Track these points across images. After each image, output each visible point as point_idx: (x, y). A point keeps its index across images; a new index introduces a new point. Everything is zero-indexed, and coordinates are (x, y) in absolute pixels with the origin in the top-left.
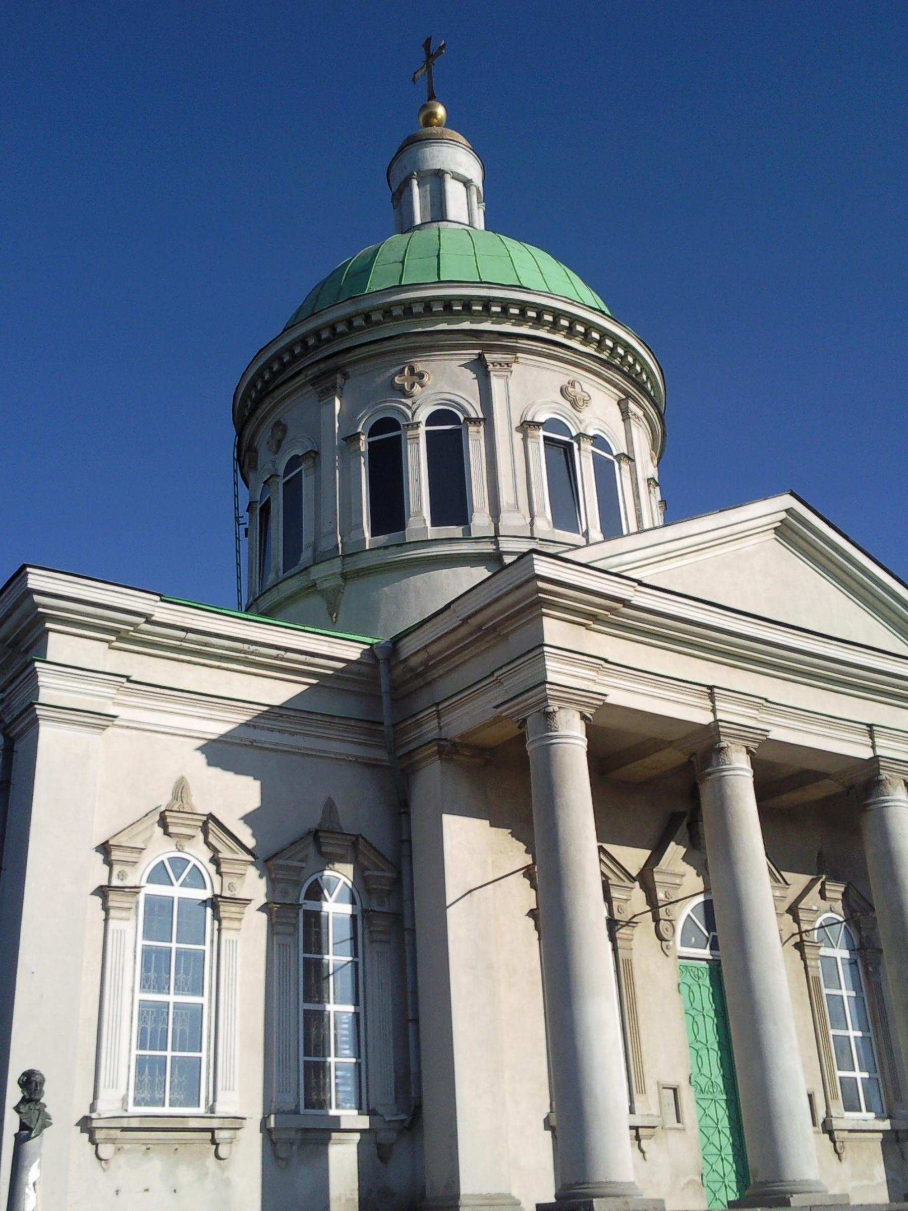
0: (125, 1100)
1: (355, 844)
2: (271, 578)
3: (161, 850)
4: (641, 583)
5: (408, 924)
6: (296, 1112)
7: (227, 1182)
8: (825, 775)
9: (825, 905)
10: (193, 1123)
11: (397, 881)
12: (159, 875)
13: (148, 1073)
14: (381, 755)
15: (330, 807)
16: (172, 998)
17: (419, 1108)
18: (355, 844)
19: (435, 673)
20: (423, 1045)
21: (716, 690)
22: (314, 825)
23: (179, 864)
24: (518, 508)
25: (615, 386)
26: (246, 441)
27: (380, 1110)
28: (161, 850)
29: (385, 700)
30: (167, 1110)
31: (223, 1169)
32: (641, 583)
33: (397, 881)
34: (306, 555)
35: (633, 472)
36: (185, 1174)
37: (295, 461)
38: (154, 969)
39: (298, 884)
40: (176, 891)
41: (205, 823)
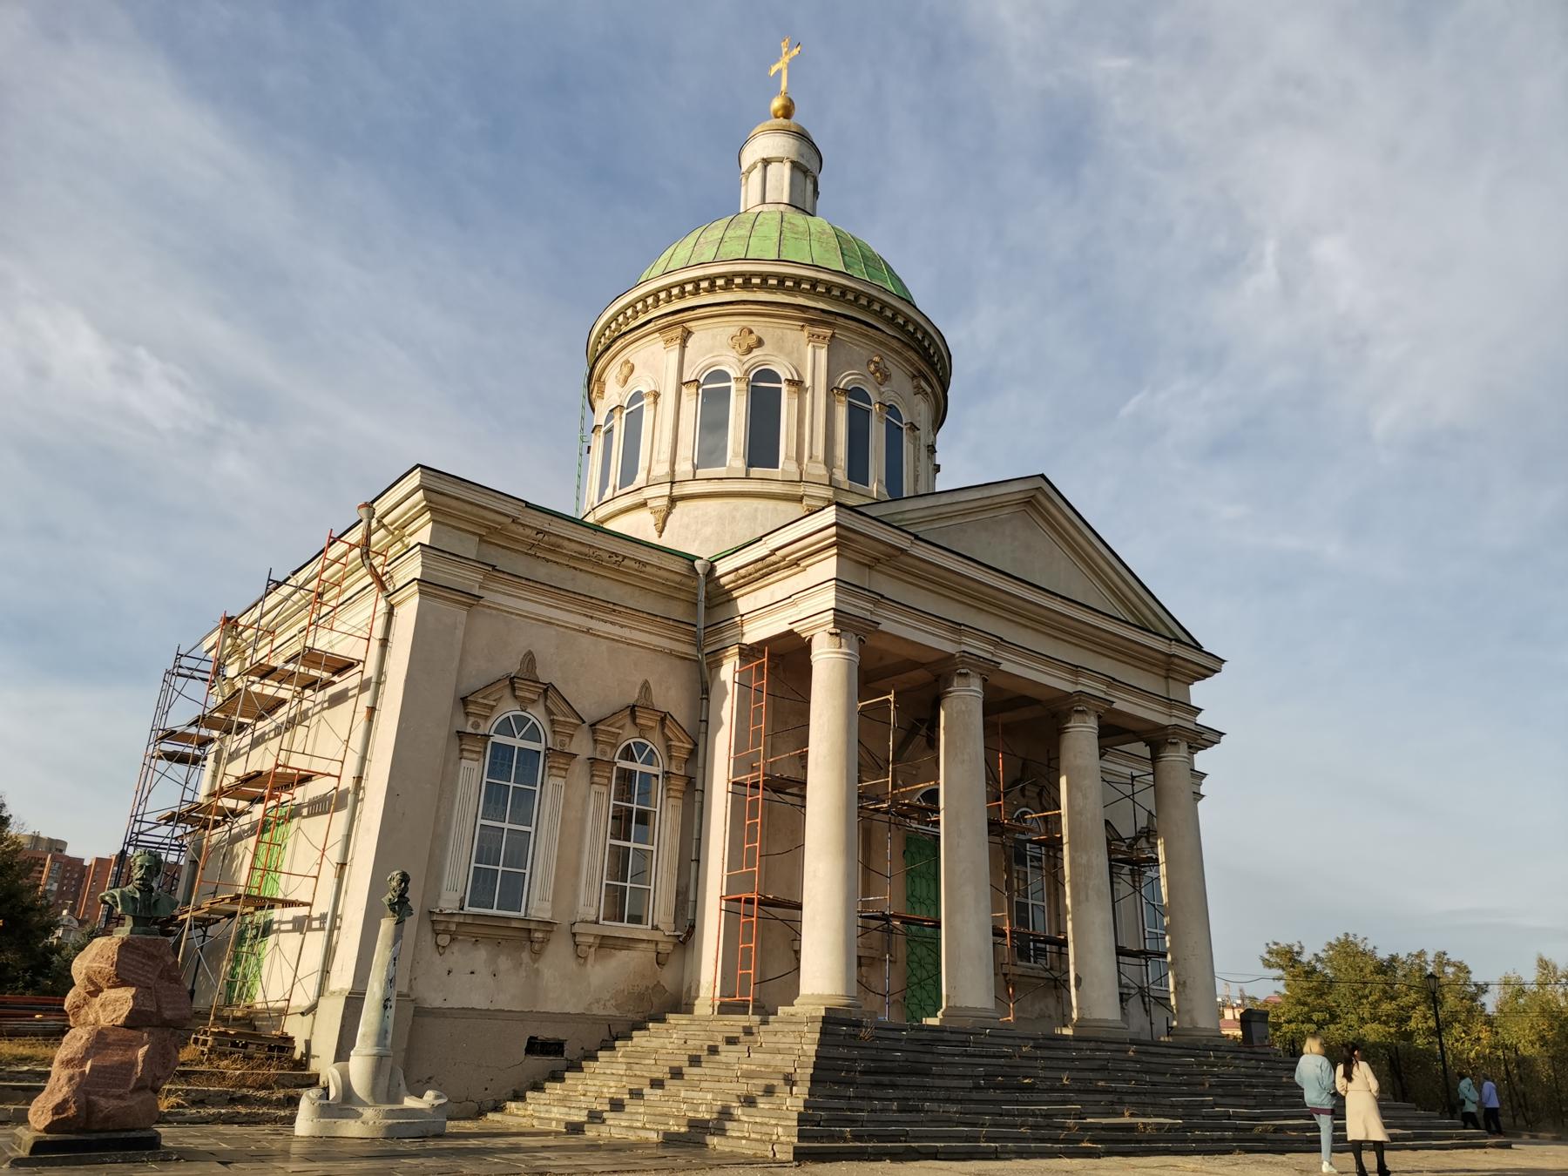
0: (462, 900)
1: (663, 720)
2: (608, 493)
3: (509, 709)
4: (917, 537)
5: (699, 787)
6: (597, 922)
7: (537, 971)
8: (1038, 702)
9: (1023, 801)
10: (514, 924)
11: (693, 753)
12: (505, 728)
13: (482, 883)
14: (690, 650)
15: (646, 687)
16: (506, 825)
17: (693, 927)
18: (663, 720)
19: (735, 594)
20: (1041, 636)
21: (341, 817)
22: (631, 702)
23: (522, 721)
24: (626, 381)
25: (912, 365)
26: (597, 372)
27: (661, 926)
28: (509, 709)
29: (702, 606)
30: (495, 912)
31: (535, 961)
32: (917, 537)
33: (693, 753)
34: (640, 479)
35: (916, 439)
36: (504, 963)
37: (638, 397)
38: (494, 799)
39: (615, 746)
40: (517, 742)
41: (546, 691)
